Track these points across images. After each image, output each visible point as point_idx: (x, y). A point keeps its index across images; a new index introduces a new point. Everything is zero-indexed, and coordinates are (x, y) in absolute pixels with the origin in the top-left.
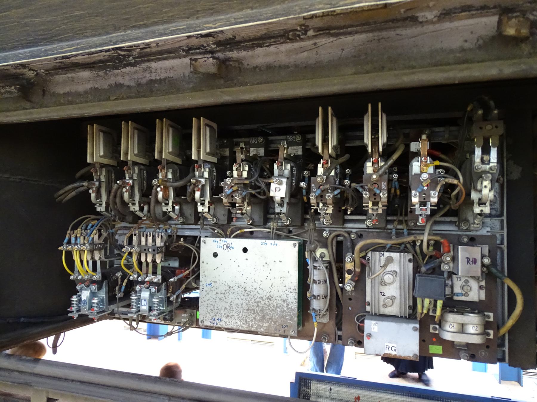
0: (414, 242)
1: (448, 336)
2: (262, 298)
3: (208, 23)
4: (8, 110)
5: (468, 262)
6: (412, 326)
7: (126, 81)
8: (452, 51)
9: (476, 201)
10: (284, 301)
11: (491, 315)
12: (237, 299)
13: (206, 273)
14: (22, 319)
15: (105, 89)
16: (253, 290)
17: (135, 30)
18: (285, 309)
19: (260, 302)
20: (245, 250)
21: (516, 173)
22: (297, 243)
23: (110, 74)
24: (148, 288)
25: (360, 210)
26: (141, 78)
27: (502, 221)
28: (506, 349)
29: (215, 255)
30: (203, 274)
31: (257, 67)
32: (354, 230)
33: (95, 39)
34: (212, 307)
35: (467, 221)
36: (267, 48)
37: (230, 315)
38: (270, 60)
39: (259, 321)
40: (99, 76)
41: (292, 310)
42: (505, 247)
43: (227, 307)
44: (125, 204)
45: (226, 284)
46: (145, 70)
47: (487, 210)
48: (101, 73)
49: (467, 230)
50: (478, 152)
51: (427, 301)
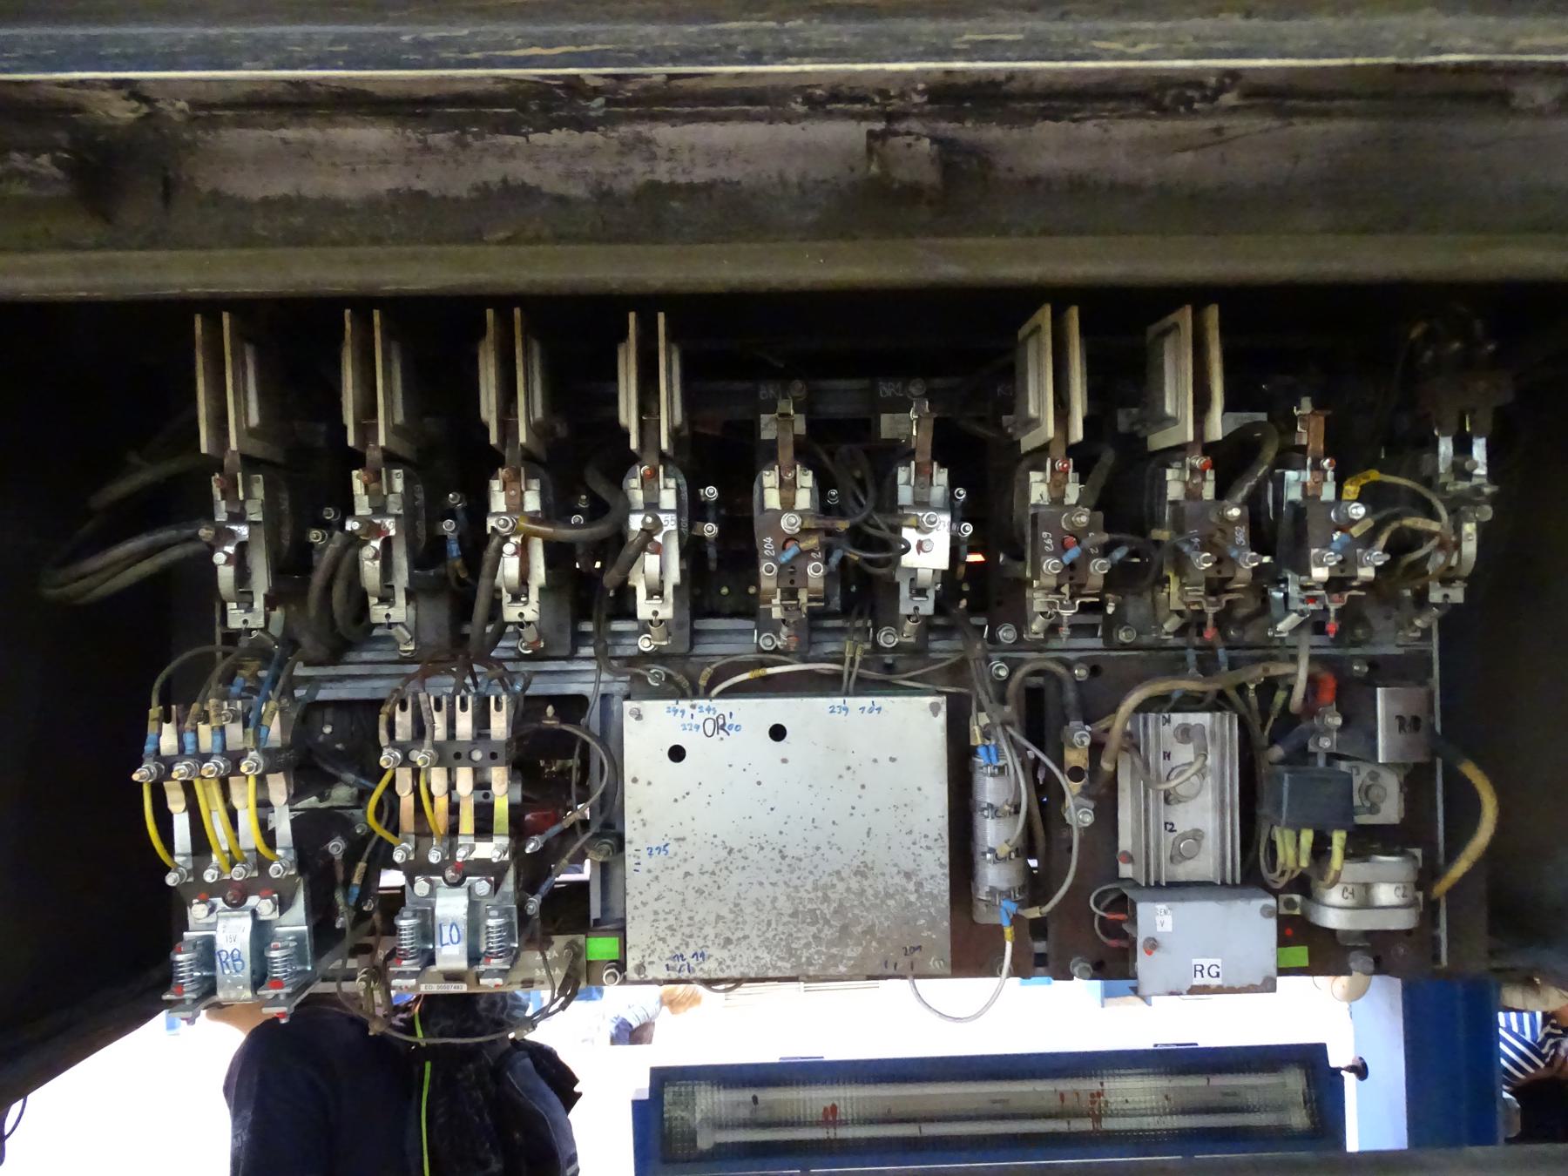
2: (838, 873)
3: (1100, 36)
5: (1401, 728)
7: (548, 178)
10: (908, 876)
12: (756, 886)
13: (645, 815)
15: (457, 200)
16: (810, 851)
17: (824, 21)
18: (913, 898)
19: (834, 886)
20: (778, 733)
22: (942, 700)
23: (477, 144)
24: (458, 884)
25: (749, 609)
26: (615, 176)
30: (637, 818)
33: (652, 30)
34: (671, 920)
36: (1073, 125)
37: (734, 938)
38: (1077, 162)
39: (831, 944)
40: (427, 148)
43: (725, 912)
45: (717, 841)
46: (627, 148)
48: (439, 139)
50: (1446, 447)
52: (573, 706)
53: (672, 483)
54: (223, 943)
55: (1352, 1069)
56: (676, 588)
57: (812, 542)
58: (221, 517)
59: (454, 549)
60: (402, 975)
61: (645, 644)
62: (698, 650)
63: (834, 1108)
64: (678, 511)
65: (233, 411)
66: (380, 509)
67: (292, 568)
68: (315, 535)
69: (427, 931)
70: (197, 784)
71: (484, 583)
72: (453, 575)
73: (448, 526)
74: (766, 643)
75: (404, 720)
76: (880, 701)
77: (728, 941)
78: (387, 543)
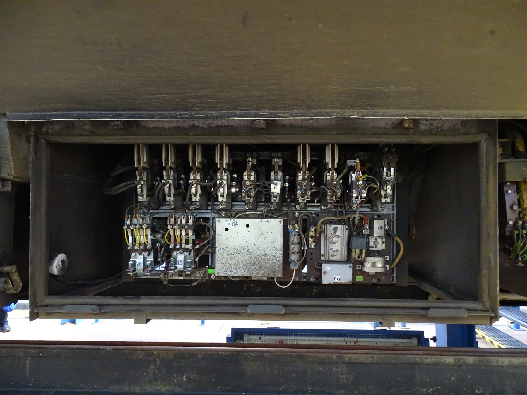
0: (349, 219)
1: (366, 270)
4: (107, 135)
6: (348, 265)
8: (381, 128)
9: (383, 195)
10: (274, 256)
11: (388, 257)
14: (79, 282)
20: (248, 226)
21: (400, 180)
27: (393, 206)
28: (395, 275)
29: (227, 229)
31: (284, 125)
32: (313, 212)
34: (225, 264)
35: (377, 206)
39: (257, 270)
41: (279, 261)
42: (395, 220)
44: (164, 196)
47: (388, 200)
49: (376, 211)
50: (385, 169)
51: (358, 250)
52: (206, 220)
53: (226, 174)
54: (137, 261)
55: (431, 339)
56: (226, 195)
57: (252, 187)
58: (138, 179)
59: (183, 186)
60: (171, 270)
61: (221, 207)
62: (233, 209)
63: (282, 341)
64: (227, 180)
65: (142, 159)
66: (168, 179)
67: (151, 189)
68: (155, 183)
69: (176, 262)
70: (134, 229)
71: (188, 194)
72: (182, 192)
73: (182, 182)
74: (246, 207)
75: (172, 220)
76: (269, 220)
77: (236, 268)
78: (170, 185)
